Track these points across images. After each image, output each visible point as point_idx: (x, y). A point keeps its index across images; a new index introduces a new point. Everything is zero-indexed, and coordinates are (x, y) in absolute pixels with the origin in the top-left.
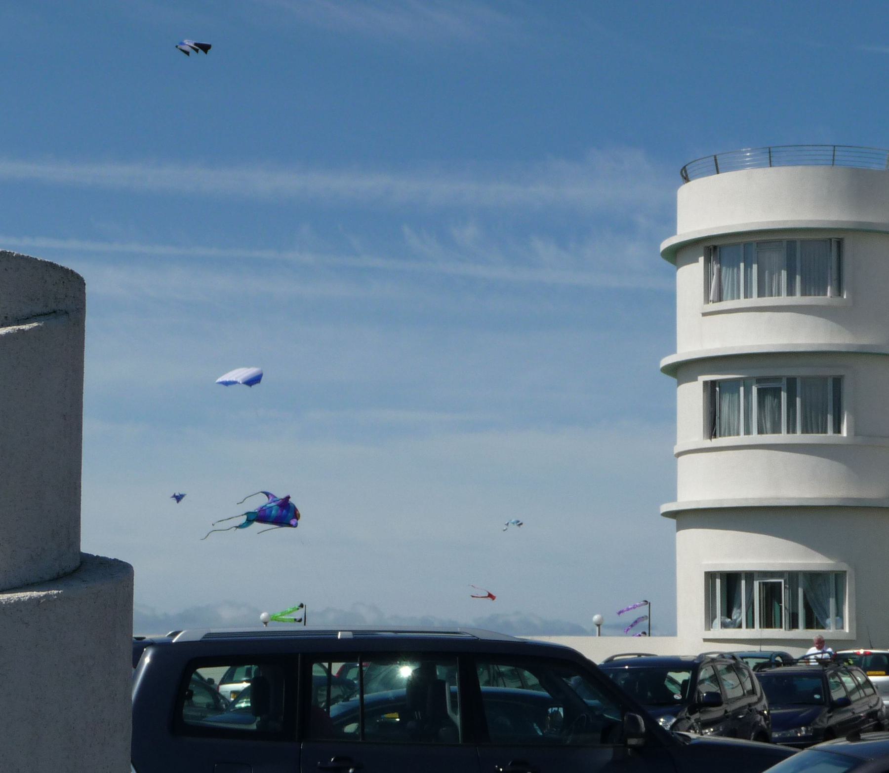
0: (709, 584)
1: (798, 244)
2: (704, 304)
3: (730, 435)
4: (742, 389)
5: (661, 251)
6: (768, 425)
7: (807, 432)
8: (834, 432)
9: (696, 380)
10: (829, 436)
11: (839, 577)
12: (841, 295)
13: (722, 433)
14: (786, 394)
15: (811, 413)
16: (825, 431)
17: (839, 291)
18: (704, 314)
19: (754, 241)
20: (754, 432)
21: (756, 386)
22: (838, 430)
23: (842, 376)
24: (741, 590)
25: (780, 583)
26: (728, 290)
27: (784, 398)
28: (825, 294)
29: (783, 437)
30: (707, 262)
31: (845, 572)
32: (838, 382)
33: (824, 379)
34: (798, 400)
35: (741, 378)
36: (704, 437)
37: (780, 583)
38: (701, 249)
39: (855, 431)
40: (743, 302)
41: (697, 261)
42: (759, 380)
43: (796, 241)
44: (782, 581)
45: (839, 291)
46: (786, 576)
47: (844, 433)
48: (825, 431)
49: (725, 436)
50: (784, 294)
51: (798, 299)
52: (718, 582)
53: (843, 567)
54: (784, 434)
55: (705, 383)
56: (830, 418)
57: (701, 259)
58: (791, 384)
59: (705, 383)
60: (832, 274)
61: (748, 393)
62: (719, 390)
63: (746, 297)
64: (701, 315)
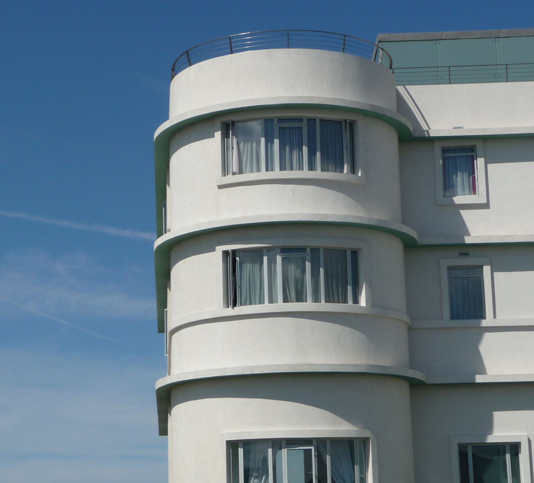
0: (231, 474)
1: (322, 252)
2: (222, 176)
3: (251, 304)
4: (265, 259)
5: (156, 388)
6: (293, 294)
7: (330, 302)
8: (353, 303)
9: (214, 250)
10: (348, 307)
11: (365, 441)
12: (355, 173)
13: (243, 303)
14: (307, 148)
15: (332, 283)
16: (345, 301)
17: (353, 170)
18: (220, 187)
19: (276, 117)
20: (276, 169)
21: (280, 256)
22: (356, 301)
23: (359, 249)
24: (268, 464)
25: (311, 450)
26: (247, 160)
27: (309, 278)
28: (342, 171)
29: (308, 306)
30: (225, 136)
31: (369, 438)
32: (355, 254)
33: (343, 252)
34: (322, 270)
35: (265, 247)
36: (223, 306)
37: (311, 450)
38: (218, 123)
39: (365, 173)
40: (264, 175)
41: (213, 136)
42: (284, 250)
43: (319, 249)
44: (313, 448)
45: (353, 170)
46: (315, 443)
47: (363, 302)
48: (345, 301)
49: (245, 304)
50: (309, 300)
51: (318, 174)
52: (241, 451)
53: (366, 434)
54: (309, 302)
55: (226, 253)
56: (350, 289)
57: (218, 135)
58: (315, 251)
59: (226, 253)
60: (346, 156)
61: (272, 262)
62: (239, 259)
63: (267, 170)
64: (217, 187)
